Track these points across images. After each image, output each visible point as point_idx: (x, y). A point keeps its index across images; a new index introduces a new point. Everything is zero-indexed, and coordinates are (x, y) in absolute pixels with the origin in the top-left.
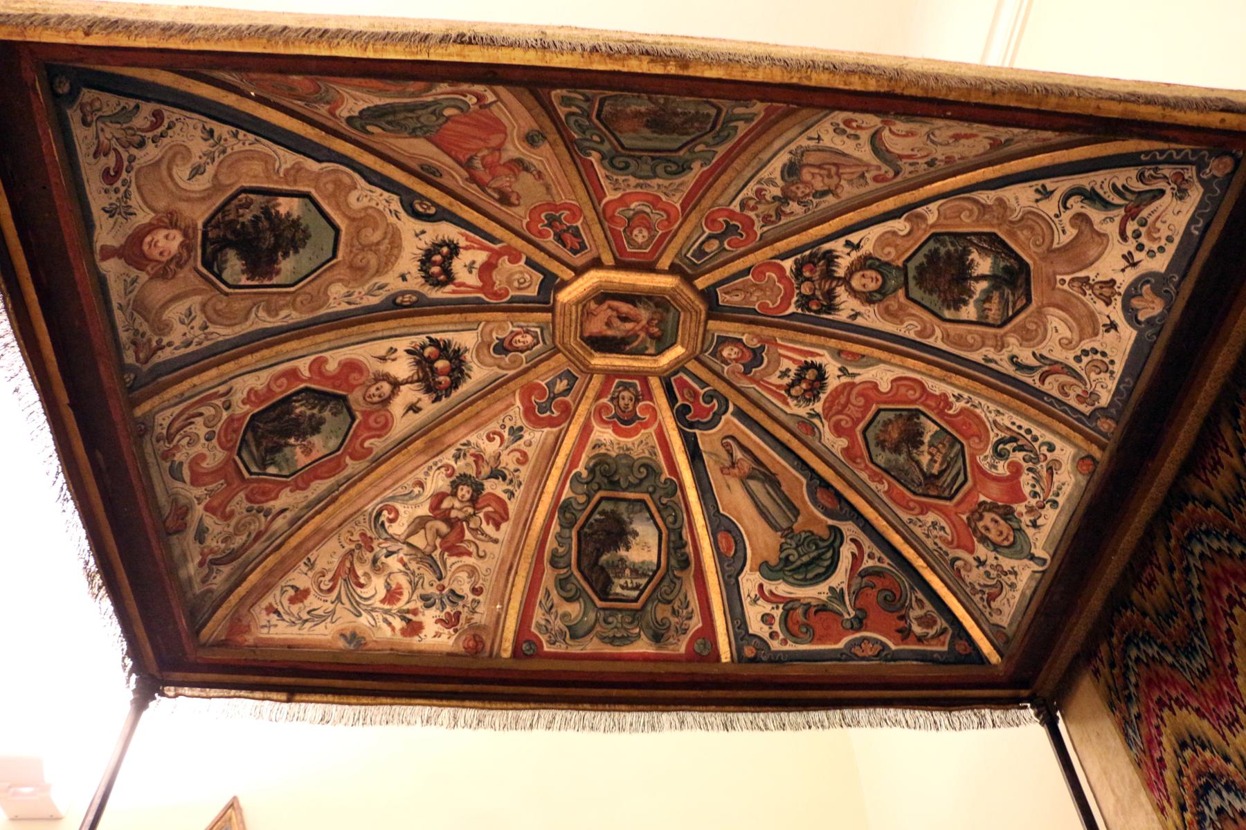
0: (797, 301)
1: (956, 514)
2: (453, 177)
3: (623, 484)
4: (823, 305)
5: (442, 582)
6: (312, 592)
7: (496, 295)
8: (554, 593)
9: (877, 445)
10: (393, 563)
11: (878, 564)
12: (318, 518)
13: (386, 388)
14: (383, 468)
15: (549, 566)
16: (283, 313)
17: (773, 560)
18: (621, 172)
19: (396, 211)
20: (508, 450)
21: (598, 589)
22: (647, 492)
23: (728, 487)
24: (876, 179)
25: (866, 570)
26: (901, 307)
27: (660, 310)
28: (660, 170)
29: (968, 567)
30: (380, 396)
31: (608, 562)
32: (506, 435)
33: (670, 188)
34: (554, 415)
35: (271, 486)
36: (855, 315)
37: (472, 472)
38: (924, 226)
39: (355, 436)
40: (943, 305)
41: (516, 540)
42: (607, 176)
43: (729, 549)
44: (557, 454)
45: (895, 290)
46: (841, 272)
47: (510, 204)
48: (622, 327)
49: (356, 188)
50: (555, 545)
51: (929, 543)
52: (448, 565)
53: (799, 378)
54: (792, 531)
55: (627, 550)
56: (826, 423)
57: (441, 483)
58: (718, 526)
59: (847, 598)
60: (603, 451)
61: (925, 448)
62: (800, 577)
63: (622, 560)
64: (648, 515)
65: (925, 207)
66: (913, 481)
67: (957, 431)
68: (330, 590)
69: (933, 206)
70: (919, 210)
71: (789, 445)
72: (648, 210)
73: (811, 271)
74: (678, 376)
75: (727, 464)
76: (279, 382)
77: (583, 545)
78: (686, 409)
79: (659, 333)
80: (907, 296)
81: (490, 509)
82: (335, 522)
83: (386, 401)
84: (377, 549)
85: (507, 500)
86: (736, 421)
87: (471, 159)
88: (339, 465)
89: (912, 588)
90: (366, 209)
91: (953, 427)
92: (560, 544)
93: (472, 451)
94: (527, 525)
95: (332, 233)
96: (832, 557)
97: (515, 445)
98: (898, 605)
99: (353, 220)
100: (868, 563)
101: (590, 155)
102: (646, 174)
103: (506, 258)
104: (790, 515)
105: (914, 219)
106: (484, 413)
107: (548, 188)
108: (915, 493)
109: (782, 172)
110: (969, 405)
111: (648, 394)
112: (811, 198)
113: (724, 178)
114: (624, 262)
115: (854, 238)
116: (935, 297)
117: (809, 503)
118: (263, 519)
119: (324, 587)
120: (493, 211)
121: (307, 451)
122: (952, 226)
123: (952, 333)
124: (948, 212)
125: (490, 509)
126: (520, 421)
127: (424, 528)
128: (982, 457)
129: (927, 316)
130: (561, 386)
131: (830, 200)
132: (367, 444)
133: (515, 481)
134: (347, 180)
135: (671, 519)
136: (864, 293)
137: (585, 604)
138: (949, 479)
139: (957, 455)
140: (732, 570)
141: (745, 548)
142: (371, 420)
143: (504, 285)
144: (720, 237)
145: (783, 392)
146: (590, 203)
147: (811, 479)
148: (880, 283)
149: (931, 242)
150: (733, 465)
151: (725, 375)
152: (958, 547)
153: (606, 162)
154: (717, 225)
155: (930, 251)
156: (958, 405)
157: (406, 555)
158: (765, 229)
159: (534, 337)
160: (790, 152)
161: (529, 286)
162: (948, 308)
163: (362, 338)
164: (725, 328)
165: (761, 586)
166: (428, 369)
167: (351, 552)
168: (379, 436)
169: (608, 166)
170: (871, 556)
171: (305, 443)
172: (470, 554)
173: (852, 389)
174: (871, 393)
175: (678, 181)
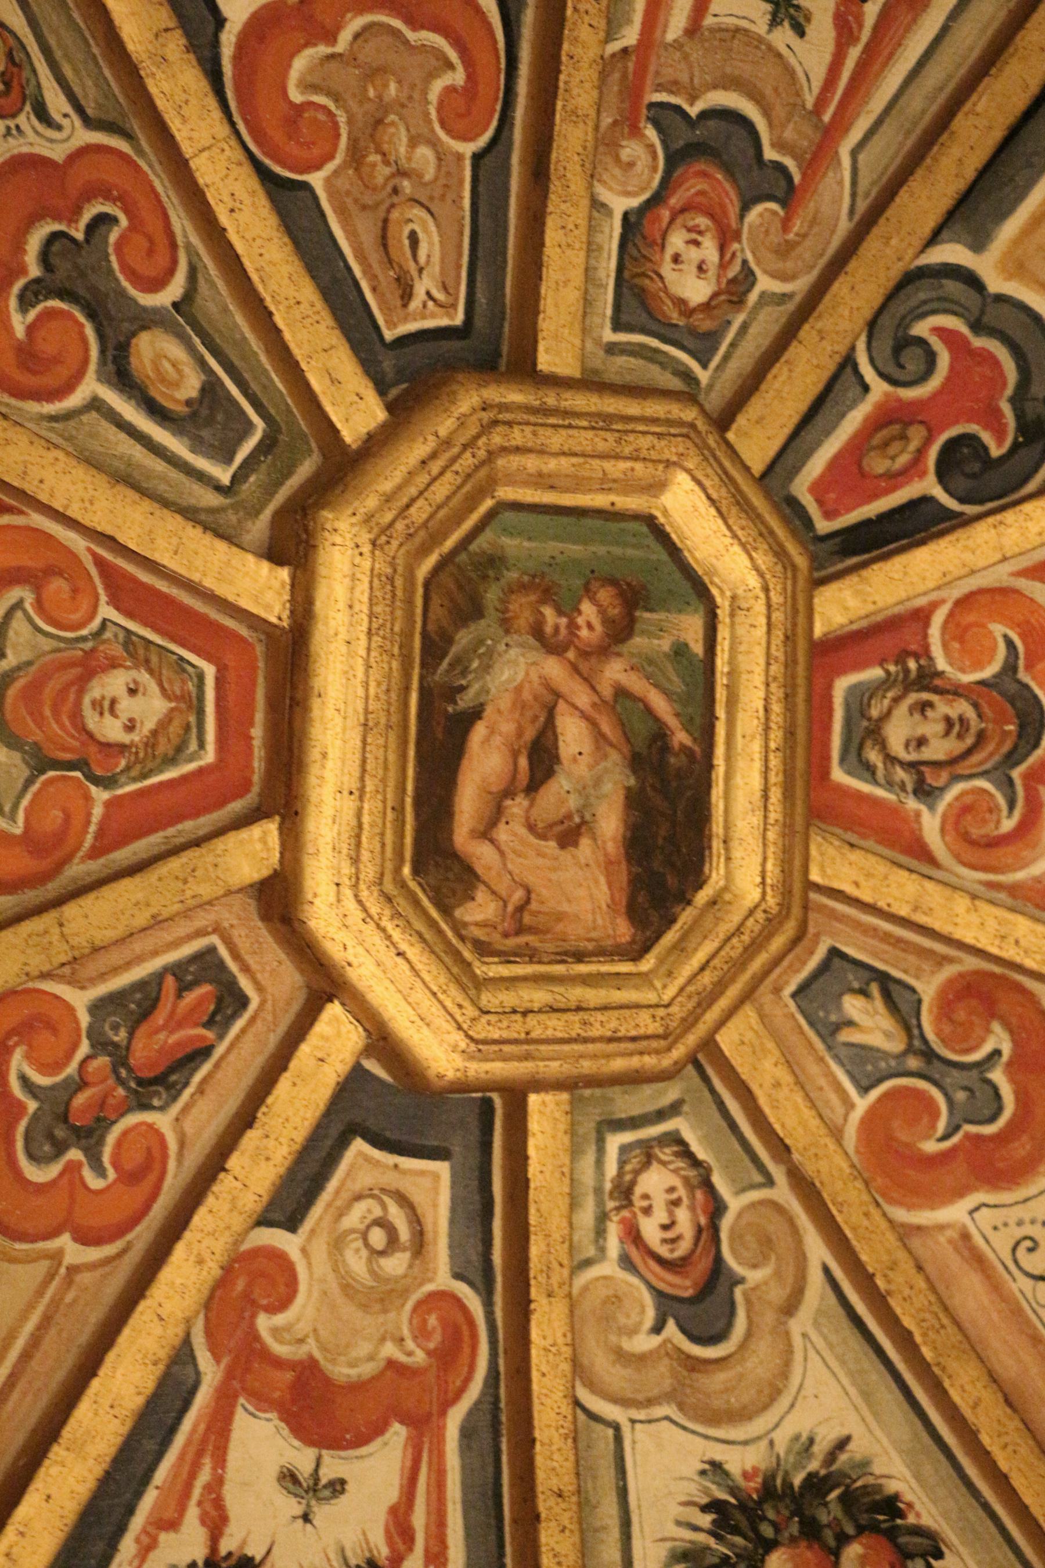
27: (492, 595)
34: (1007, 1048)
48: (582, 769)
79: (605, 595)
103: (264, 1323)
106: (1007, 1366)
114: (270, 776)
143: (402, 1319)
151: (800, 286)
154: (47, 346)
158: (56, 102)
159: (648, 1159)
161: (403, 1200)
164: (572, 296)
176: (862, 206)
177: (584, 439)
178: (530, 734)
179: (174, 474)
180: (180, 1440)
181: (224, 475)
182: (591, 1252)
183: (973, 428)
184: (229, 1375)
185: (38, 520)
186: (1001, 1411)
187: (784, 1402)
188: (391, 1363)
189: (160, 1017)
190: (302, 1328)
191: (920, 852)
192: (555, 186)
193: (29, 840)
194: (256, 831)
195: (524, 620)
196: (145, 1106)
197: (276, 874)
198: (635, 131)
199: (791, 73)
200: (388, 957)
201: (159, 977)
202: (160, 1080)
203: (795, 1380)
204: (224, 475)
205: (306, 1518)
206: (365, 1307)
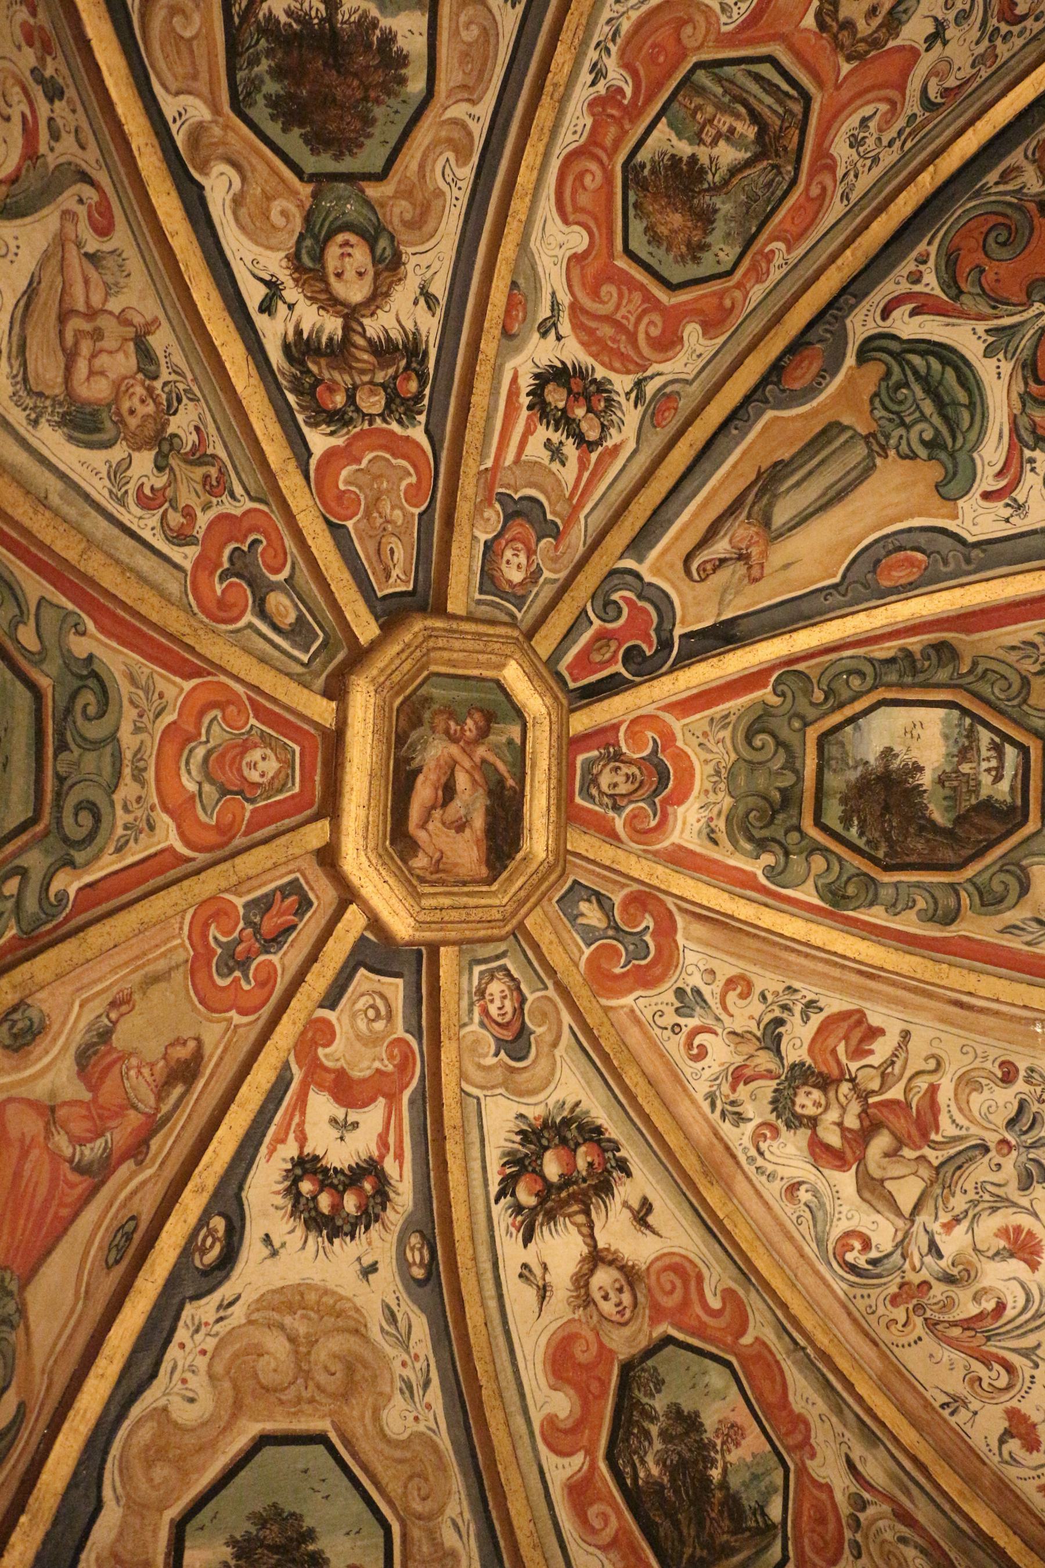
0: (400, 422)
1: (838, 87)
2: (134, 1193)
3: (787, 780)
4: (407, 367)
5: (992, 1145)
6: (1014, 1403)
7: (404, 1066)
8: (1012, 917)
9: (696, 260)
10: (953, 1243)
11: (931, 263)
12: (862, 1389)
13: (603, 1278)
14: (762, 1264)
15: (953, 927)
16: (449, 1538)
17: (934, 472)
18: (104, 825)
19: (220, 1307)
20: (724, 1016)
21: (1000, 829)
22: (802, 730)
23: (787, 566)
24: (104, 230)
25: (944, 286)
26: (406, 193)
27: (427, 715)
28: (94, 731)
29: (943, 66)
30: (620, 1290)
31: (947, 809)
32: (692, 1023)
33: (144, 703)
34: (652, 925)
35: (806, 1505)
36: (430, 300)
37: (767, 1088)
38: (217, 131)
39: (699, 1331)
40: (397, 95)
41: (900, 993)
42: (118, 850)
43: (912, 563)
44: (731, 917)
45: (367, 203)
46: (332, 325)
47: (198, 1056)
48: (466, 797)
49: (165, 1409)
50: (912, 915)
51: (889, 158)
52: (957, 1132)
53: (564, 421)
54: (873, 435)
55: (921, 769)
56: (655, 368)
57: (791, 1149)
58: (867, 586)
59: (1007, 321)
60: (721, 824)
61: (703, 154)
62: (966, 415)
63: (941, 781)
64: (849, 729)
65: (174, 128)
66: (769, 184)
67: (669, 75)
68: (1010, 1368)
69: (169, 106)
70: (180, 140)
71: (699, 445)
72: (200, 752)
73: (331, 390)
74: (566, 674)
75: (741, 569)
76: (597, 1524)
77: (913, 859)
78: (632, 656)
79: (477, 716)
80: (381, 177)
81: (841, 1049)
82: (866, 1349)
83: (630, 1275)
84: (925, 1275)
85: (822, 1016)
86: (654, 554)
87: (80, 1169)
88: (759, 1357)
89: (977, 194)
90: (212, 1377)
91: (660, 85)
92: (911, 905)
93: (726, 1088)
94: (871, 973)
95: (269, 1452)
96: (923, 354)
97: (714, 1003)
98: (1017, 216)
99: (238, 1408)
100: (931, 283)
101: (62, 896)
102: (107, 760)
103: (321, 1052)
104: (842, 439)
105: (204, 153)
106: (650, 1069)
107: (155, 979)
108: (793, 182)
109: (90, 446)
110: (614, 49)
111: (604, 735)
112: (158, 384)
113: (109, 578)
114: (324, 798)
115: (253, 294)
116: (378, 112)
117: (815, 403)
118: (871, 1511)
119: (1003, 1380)
120: (218, 1088)
121: (733, 1433)
122: (211, 55)
123: (458, 78)
124: (180, 70)
125: (841, 1049)
126: (665, 996)
127: (882, 1181)
128: (724, 19)
129: (423, 135)
130: (591, 915)
131: (161, 341)
132: (715, 1303)
133: (784, 999)
134: (146, 1434)
135: (856, 682)
136: (377, 275)
137: (1034, 854)
138: (769, 100)
139: (719, 80)
140: (955, 555)
141: (910, 530)
142: (669, 1302)
143: (382, 1051)
144: (260, 591)
145: (594, 456)
146: (186, 883)
147: (766, 401)
148: (353, 238)
149: (252, 113)
150: (743, 557)
151: (562, 575)
152: (902, 88)
153: (79, 857)
154: (231, 598)
155: (273, 118)
156: (615, 74)
157: (936, 1218)
158: (238, 490)
159: (492, 977)
160: (35, 423)
161: (382, 996)
162: (402, 81)
163: (501, 1341)
164: (463, 578)
165: (987, 496)
166: (564, 1194)
167: (931, 1325)
168: (700, 1278)
169: (90, 851)
170: (916, 278)
171: (719, 1442)
172: (933, 1089)
173: (586, 312)
174: (593, 267)
175: (125, 688)
176: (589, 541)
177: (470, 645)
178: (443, 780)
179: (283, 658)
180: (285, 1103)
181: (305, 658)
182: (466, 1020)
183: (638, 642)
184: (306, 1076)
185: (223, 679)
186: (647, 1087)
187: (552, 1086)
188: (378, 1071)
189: (274, 911)
190: (337, 1055)
191: (615, 836)
192: (457, 529)
193: (218, 828)
194: (318, 824)
195: (441, 726)
196: (268, 952)
197: (328, 845)
198: (491, 505)
199: (558, 481)
200: (380, 884)
201: (274, 891)
202: (274, 940)
203: (557, 1075)
204: (305, 658)
205: (342, 1138)
206: (365, 1045)
